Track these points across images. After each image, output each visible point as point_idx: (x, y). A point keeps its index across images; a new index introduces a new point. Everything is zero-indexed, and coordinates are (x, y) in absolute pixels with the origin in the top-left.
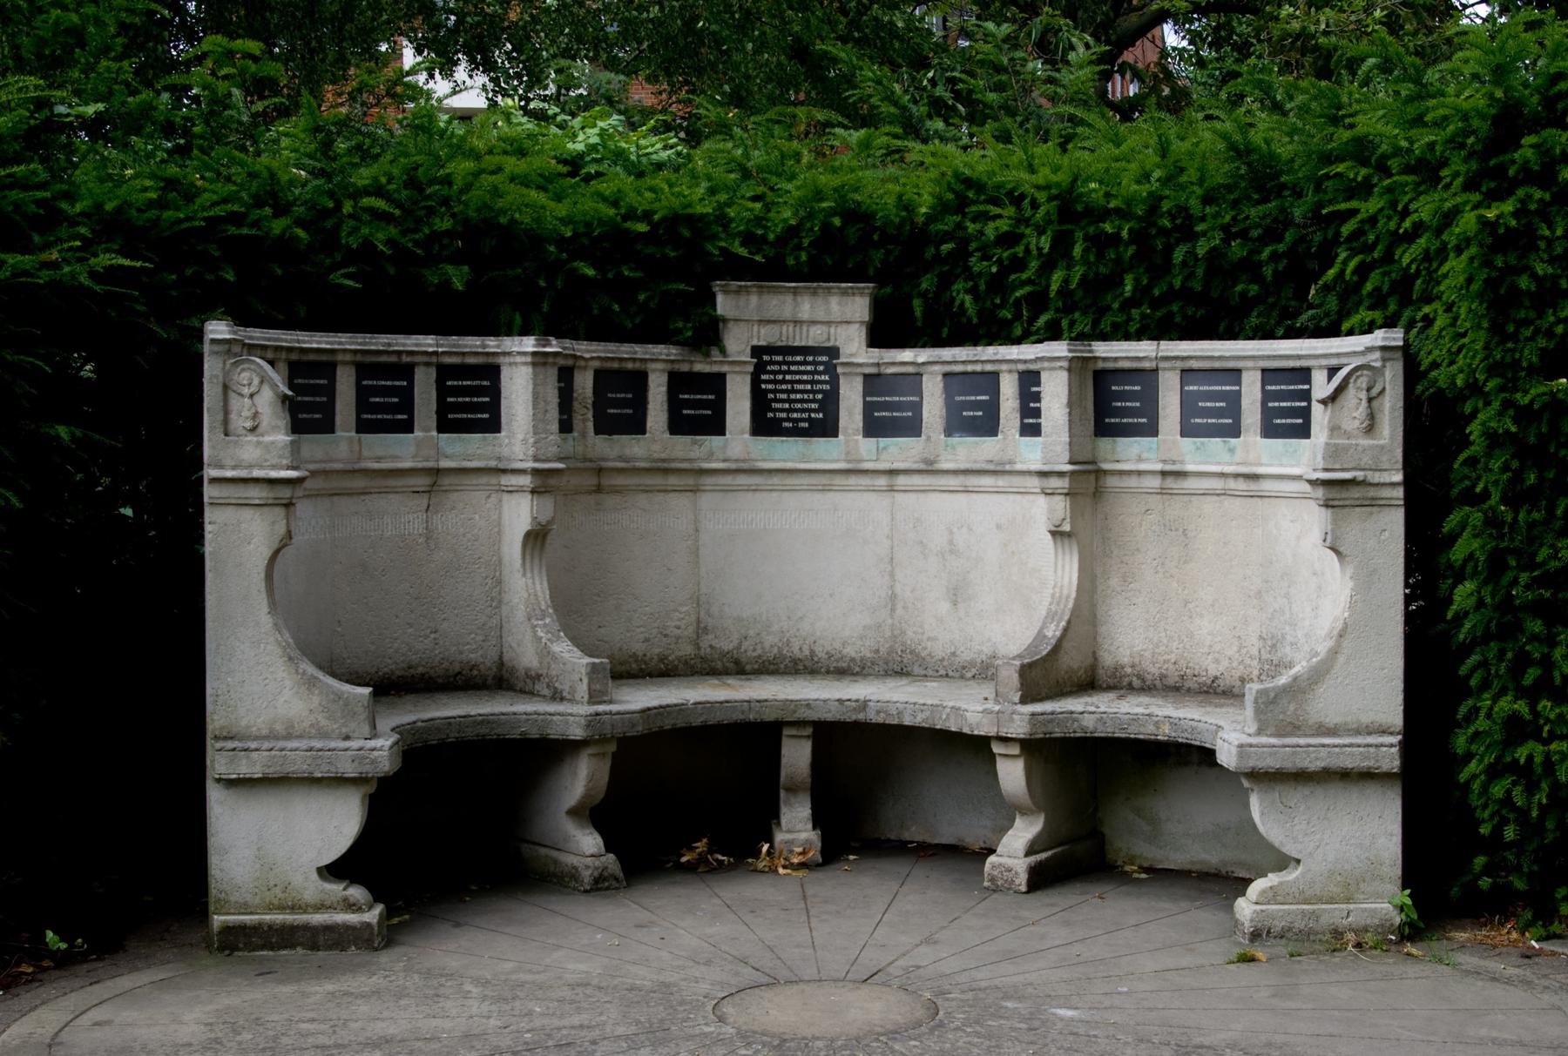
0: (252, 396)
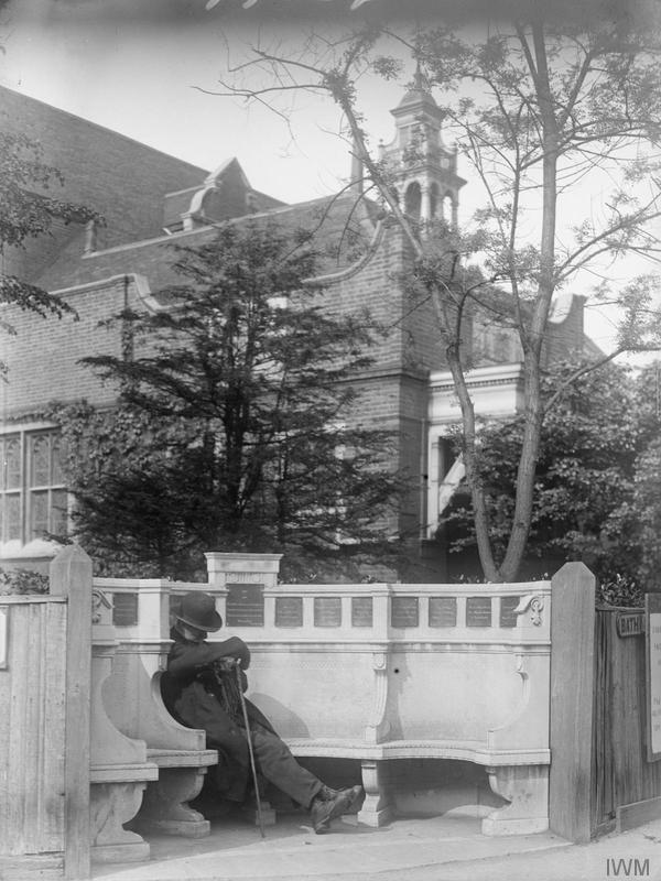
0: (540, 611)
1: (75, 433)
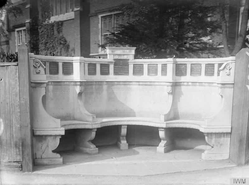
0: (230, 69)
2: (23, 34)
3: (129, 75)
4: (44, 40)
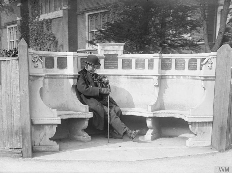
0: (211, 64)
1: (113, 13)
2: (14, 30)
3: (118, 69)
4: (34, 36)
